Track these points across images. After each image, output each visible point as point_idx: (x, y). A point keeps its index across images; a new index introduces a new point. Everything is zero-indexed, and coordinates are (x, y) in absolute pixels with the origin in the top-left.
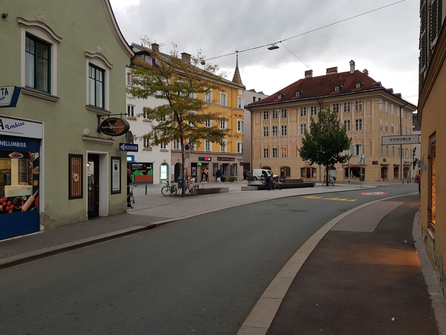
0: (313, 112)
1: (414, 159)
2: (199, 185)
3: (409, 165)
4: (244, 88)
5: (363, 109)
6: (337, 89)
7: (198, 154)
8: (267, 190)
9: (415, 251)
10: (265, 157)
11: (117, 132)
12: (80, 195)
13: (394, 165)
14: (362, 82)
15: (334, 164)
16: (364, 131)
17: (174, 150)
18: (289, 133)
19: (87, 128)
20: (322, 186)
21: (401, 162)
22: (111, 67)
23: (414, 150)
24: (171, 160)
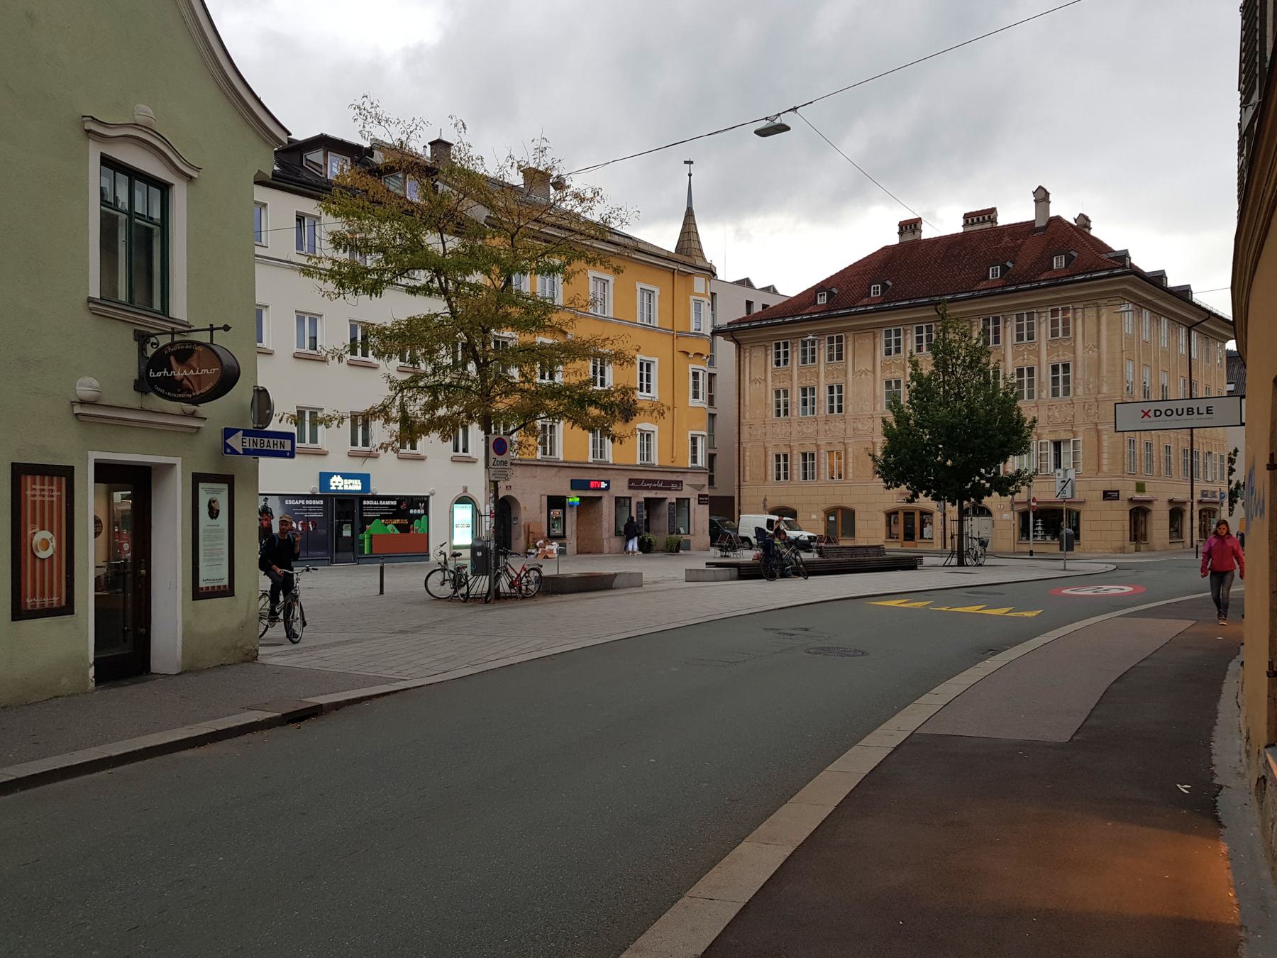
0: (922, 342)
1: (1230, 482)
2: (541, 566)
3: (1216, 503)
4: (710, 272)
5: (1075, 334)
6: (994, 273)
8: (764, 578)
9: (1217, 837)
10: (778, 478)
11: (196, 387)
12: (63, 604)
13: (1171, 501)
14: (1071, 253)
15: (983, 498)
18: (850, 408)
19: (90, 376)
20: (944, 566)
21: (1190, 492)
22: (194, 174)
23: (1232, 456)
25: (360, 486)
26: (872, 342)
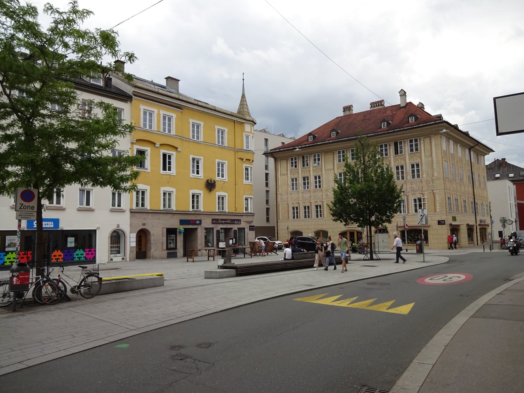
5: (421, 150)
7: (179, 215)
10: (294, 218)
16: (423, 179)
17: (136, 209)
24: (130, 225)
25: (53, 225)
26: (332, 156)
